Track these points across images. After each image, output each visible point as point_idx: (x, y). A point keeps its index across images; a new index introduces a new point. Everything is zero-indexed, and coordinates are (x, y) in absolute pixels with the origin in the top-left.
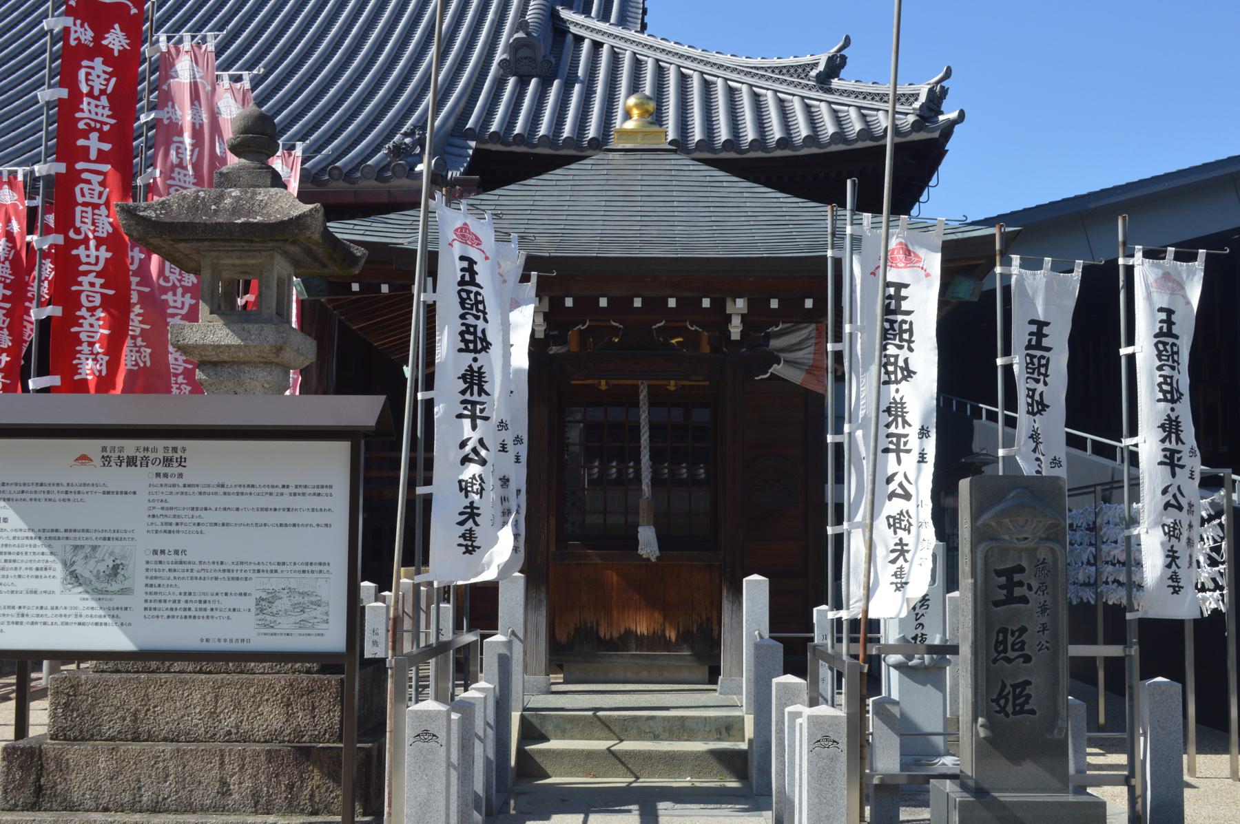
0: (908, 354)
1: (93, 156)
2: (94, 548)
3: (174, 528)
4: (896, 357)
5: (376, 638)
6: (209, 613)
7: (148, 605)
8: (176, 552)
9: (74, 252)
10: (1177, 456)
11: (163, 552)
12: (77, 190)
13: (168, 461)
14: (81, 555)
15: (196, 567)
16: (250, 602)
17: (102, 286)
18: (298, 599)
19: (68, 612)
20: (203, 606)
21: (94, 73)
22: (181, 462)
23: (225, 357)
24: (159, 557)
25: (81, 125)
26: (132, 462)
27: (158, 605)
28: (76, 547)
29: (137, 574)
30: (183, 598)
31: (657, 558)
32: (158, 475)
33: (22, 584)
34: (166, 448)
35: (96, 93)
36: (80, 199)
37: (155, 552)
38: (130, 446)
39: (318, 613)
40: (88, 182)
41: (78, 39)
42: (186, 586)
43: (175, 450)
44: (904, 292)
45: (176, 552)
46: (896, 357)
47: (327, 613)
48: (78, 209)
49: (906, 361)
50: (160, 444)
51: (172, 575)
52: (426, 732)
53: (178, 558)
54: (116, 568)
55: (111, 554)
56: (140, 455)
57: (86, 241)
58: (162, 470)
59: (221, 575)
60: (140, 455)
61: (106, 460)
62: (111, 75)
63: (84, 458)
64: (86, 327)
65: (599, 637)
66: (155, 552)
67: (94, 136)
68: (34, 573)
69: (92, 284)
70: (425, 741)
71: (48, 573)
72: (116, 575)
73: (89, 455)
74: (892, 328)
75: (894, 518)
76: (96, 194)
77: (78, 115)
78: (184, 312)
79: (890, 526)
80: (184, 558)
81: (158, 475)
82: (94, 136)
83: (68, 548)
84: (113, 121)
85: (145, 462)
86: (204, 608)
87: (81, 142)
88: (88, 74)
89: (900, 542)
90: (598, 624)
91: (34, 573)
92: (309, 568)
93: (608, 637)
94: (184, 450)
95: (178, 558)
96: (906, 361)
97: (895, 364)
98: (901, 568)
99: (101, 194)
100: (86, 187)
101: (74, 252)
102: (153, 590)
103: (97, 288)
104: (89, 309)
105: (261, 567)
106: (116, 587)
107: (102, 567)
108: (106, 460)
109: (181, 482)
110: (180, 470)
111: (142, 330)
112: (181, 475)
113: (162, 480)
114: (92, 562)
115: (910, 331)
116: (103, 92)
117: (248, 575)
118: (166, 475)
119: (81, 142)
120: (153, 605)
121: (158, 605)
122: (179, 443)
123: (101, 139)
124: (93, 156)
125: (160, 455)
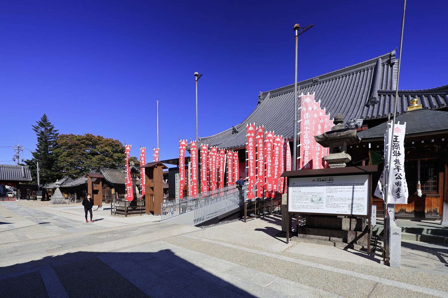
0: (399, 150)
1: (251, 150)
2: (316, 196)
3: (331, 192)
4: (396, 151)
5: (374, 211)
6: (338, 207)
7: (327, 205)
8: (332, 196)
9: (304, 147)
10: (399, 167)
11: (329, 196)
12: (304, 136)
13: (330, 180)
14: (314, 197)
15: (336, 199)
16: (347, 205)
17: (308, 153)
18: (357, 205)
19: (312, 206)
20: (337, 206)
21: (307, 115)
22: (332, 180)
23: (335, 161)
24: (328, 197)
25: (249, 146)
26: (323, 181)
27: (328, 205)
28: (313, 195)
29: (324, 200)
30: (333, 204)
31: (422, 196)
32: (328, 183)
33: (303, 202)
34: (329, 178)
35: (307, 119)
36: (305, 138)
37: (328, 196)
38: (322, 178)
39: (362, 207)
40: (306, 135)
41: (304, 110)
42: (334, 202)
43: (331, 178)
44: (397, 138)
45: (332, 196)
46: (396, 151)
47: (364, 208)
48: (304, 139)
49: (399, 152)
50: (328, 177)
51: (331, 200)
52: (396, 233)
53: (332, 197)
54: (320, 199)
55: (319, 196)
56: (324, 179)
57: (306, 145)
58: (329, 182)
59: (341, 200)
60: (324, 179)
61: (318, 181)
62: (309, 115)
63: (314, 180)
64: (306, 160)
65: (406, 212)
66: (328, 196)
67: (251, 147)
68: (306, 200)
69: (307, 152)
70: (395, 235)
71: (308, 200)
72: (320, 200)
73: (315, 180)
74: (395, 145)
75: (397, 183)
76: (307, 137)
77: (304, 123)
78: (308, 149)
79: (396, 185)
80: (333, 197)
81: (328, 183)
82: (251, 147)
83: (312, 196)
84: (310, 124)
85: (325, 180)
86: (338, 206)
87: (249, 148)
88: (306, 116)
89: (399, 188)
90: (406, 209)
91: (306, 200)
92: (360, 199)
93: (408, 212)
94: (333, 178)
95: (332, 197)
96: (399, 152)
97: (396, 152)
98: (399, 193)
99: (308, 137)
100: (306, 136)
101: (304, 147)
102: (327, 203)
103: (308, 153)
104: (306, 157)
105: (349, 199)
106: (320, 202)
107: (318, 199)
108: (318, 181)
109: (332, 184)
110: (332, 181)
111: (319, 159)
112: (332, 183)
113: (329, 184)
114: (316, 198)
115: (399, 145)
116: (308, 118)
117: (346, 200)
118: (329, 183)
119: (249, 148)
120: (327, 205)
121: (328, 205)
122: (332, 177)
123: (308, 127)
124: (251, 150)
125: (328, 179)
